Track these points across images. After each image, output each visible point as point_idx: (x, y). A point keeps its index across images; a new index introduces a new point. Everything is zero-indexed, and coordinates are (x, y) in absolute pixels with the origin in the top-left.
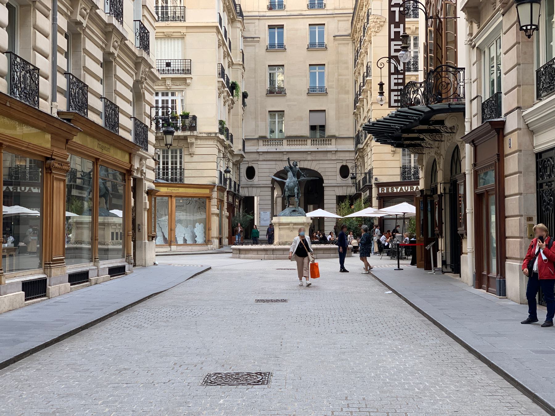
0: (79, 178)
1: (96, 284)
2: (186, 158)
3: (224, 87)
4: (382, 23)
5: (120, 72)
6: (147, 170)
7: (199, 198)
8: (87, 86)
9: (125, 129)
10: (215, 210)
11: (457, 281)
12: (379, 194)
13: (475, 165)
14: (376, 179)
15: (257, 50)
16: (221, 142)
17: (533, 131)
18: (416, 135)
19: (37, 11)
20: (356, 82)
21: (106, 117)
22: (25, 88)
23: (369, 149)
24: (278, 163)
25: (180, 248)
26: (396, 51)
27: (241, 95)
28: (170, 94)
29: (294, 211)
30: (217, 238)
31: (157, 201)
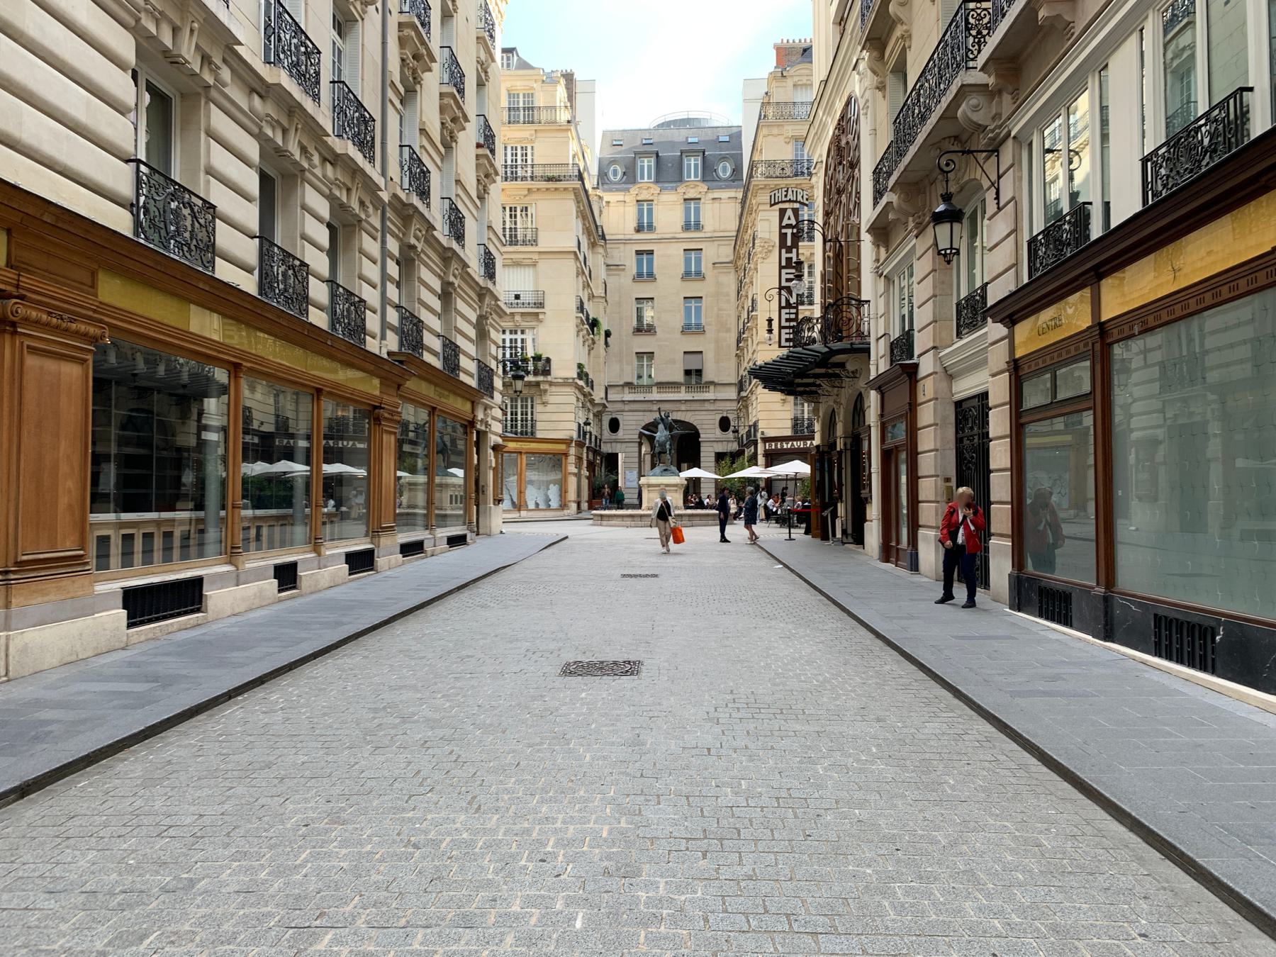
2: (538, 408)
3: (583, 324)
7: (554, 454)
10: (572, 468)
11: (859, 553)
12: (766, 450)
13: (882, 416)
14: (763, 433)
16: (580, 389)
20: (739, 317)
23: (754, 398)
25: (530, 514)
26: (788, 280)
27: (603, 333)
28: (519, 332)
30: (574, 502)
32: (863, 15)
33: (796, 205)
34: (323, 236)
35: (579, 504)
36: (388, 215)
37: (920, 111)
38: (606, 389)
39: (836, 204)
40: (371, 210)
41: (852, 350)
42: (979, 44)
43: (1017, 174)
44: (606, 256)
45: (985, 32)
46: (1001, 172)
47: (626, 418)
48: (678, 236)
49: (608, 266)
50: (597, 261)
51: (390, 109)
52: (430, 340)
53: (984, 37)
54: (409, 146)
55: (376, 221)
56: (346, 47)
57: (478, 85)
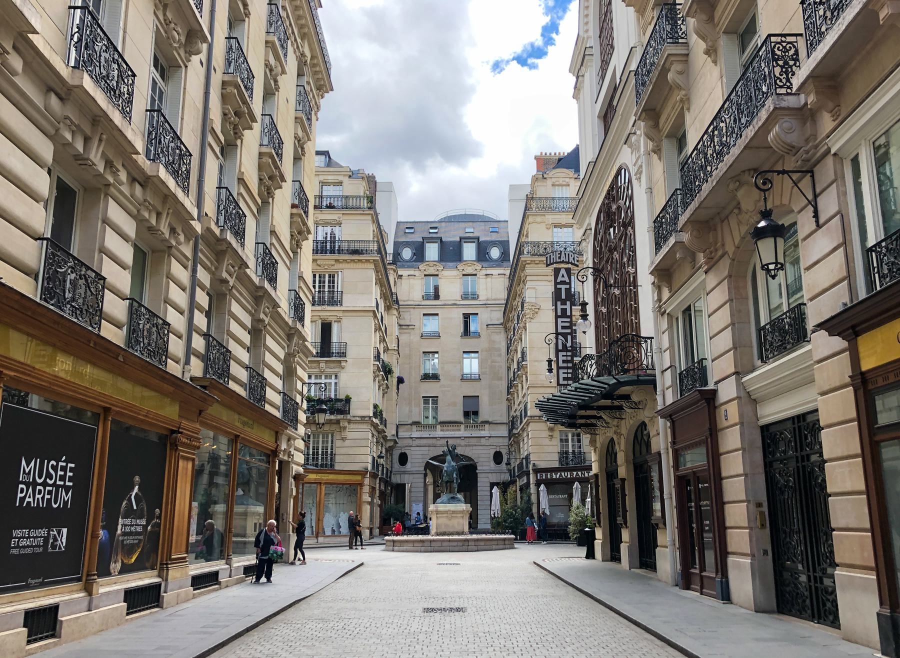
0: (223, 464)
1: (227, 586)
2: (338, 443)
3: (380, 371)
4: (537, 310)
5: (270, 342)
6: (296, 452)
7: (350, 485)
8: (230, 352)
9: (272, 405)
10: (366, 498)
11: (651, 578)
13: (674, 443)
15: (412, 338)
16: (375, 426)
17: (755, 402)
18: (594, 413)
19: (173, 259)
20: (509, 368)
21: (250, 388)
22: (149, 344)
23: (525, 434)
24: (432, 448)
25: (327, 540)
26: (563, 327)
27: (395, 381)
28: (323, 377)
29: (453, 498)
30: (368, 528)
31: (305, 488)
32: (637, 91)
33: (570, 266)
34: (127, 254)
35: (371, 530)
36: (200, 247)
37: (715, 151)
38: (397, 427)
39: (607, 262)
40: (182, 238)
41: (637, 382)
42: (787, 73)
43: (841, 189)
44: (399, 317)
45: (791, 63)
46: (818, 191)
47: (413, 453)
48: (458, 303)
49: (400, 325)
50: (391, 321)
51: (209, 155)
52: (236, 370)
53: (791, 67)
54: (226, 188)
55: (188, 251)
56: (168, 90)
57: (295, 159)
